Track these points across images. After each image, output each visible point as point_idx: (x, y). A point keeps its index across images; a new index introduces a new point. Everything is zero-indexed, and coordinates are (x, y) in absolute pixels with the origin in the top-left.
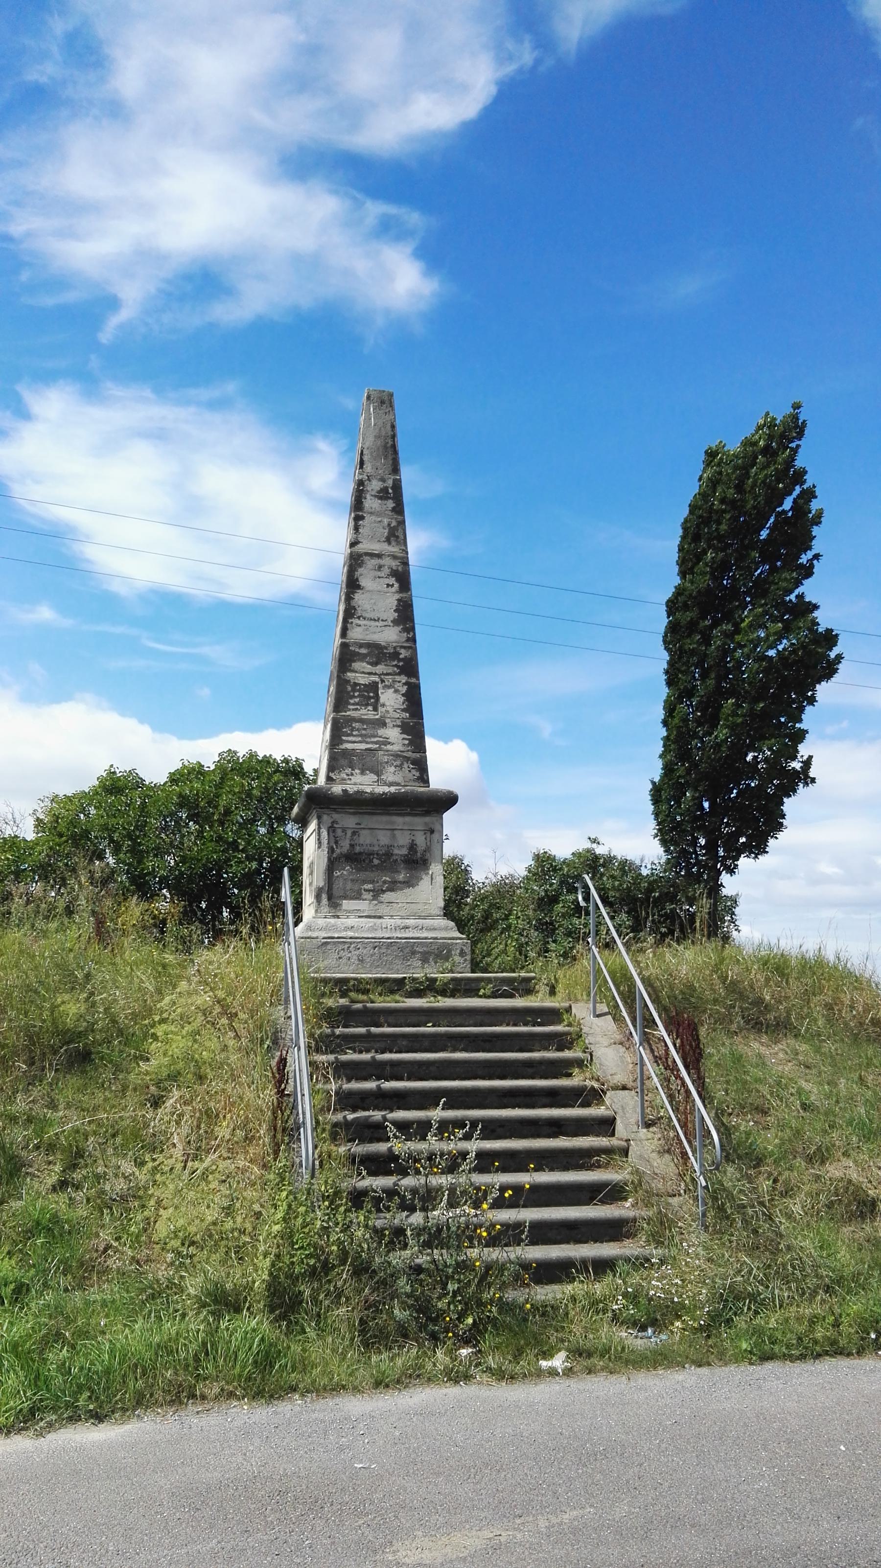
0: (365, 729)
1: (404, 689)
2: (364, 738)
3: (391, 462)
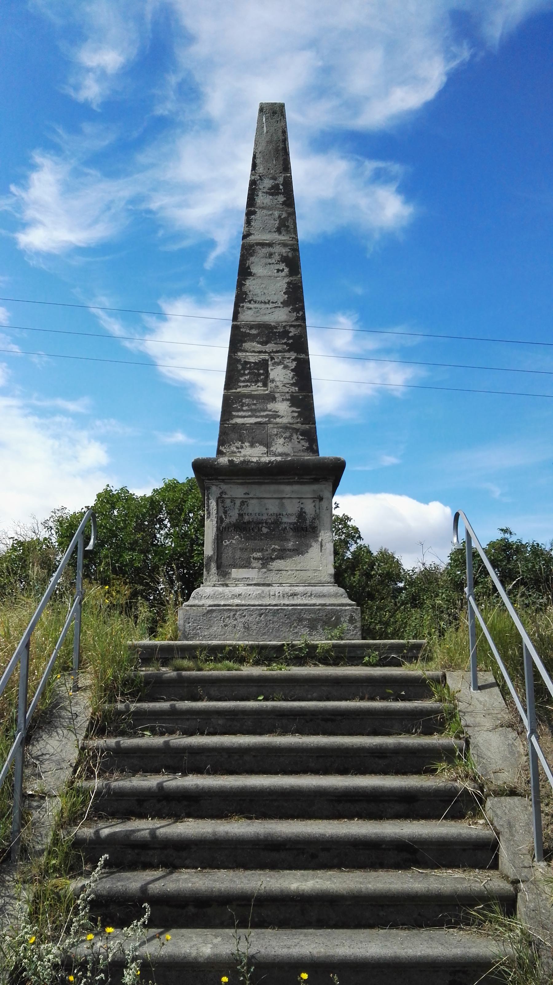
0: (255, 404)
1: (293, 365)
2: (254, 413)
3: (282, 163)
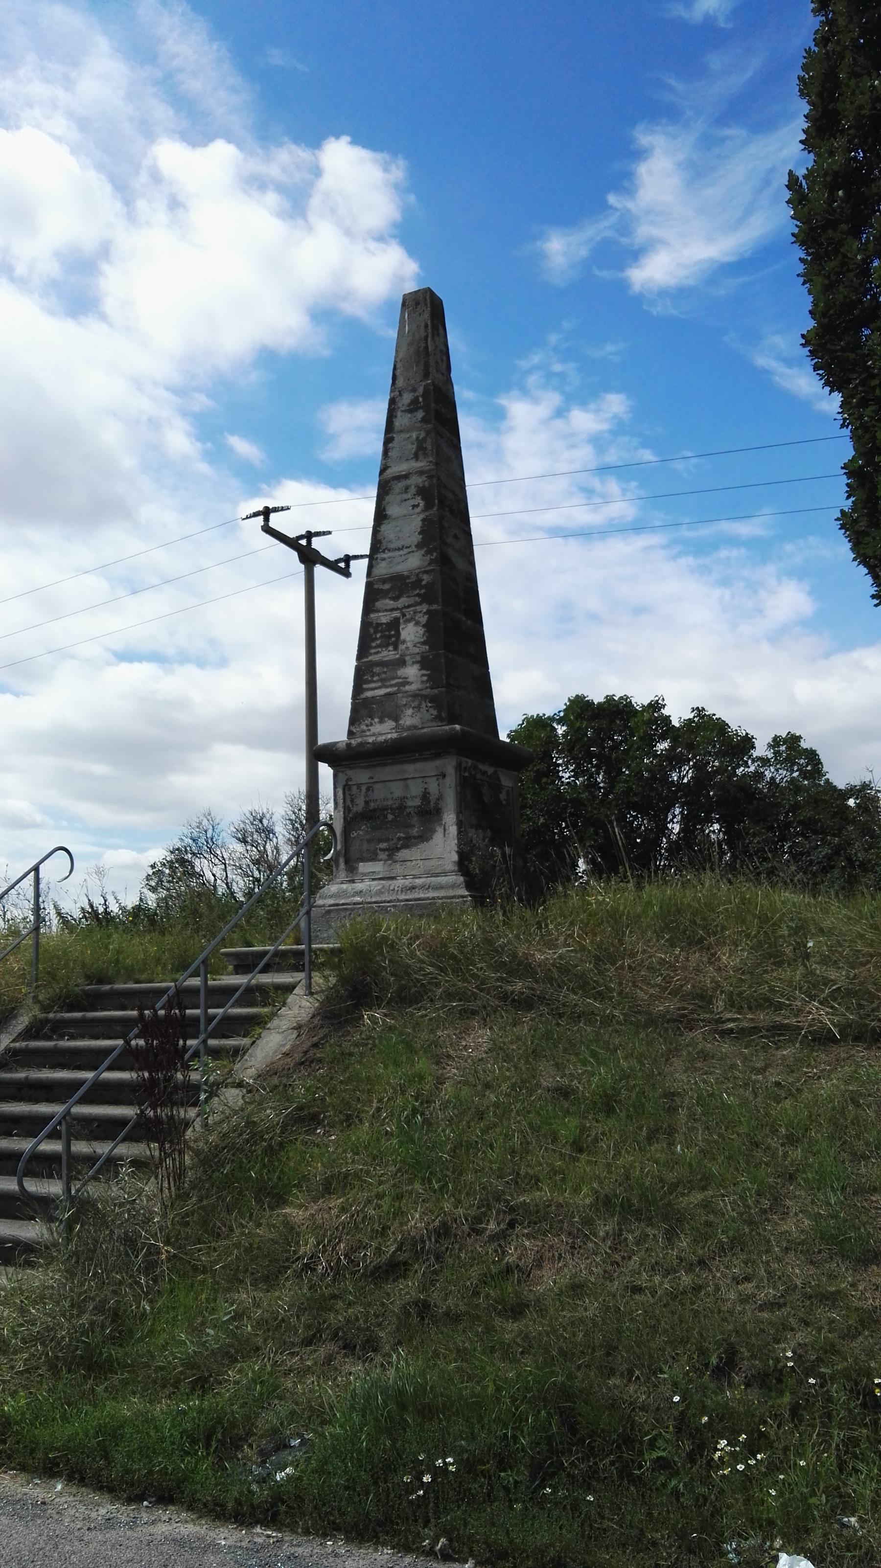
0: (385, 673)
1: (424, 619)
2: (384, 683)
